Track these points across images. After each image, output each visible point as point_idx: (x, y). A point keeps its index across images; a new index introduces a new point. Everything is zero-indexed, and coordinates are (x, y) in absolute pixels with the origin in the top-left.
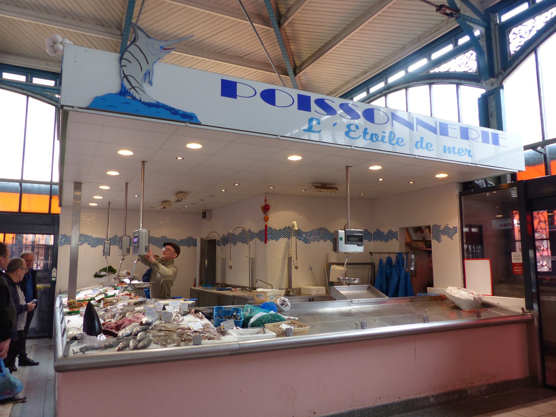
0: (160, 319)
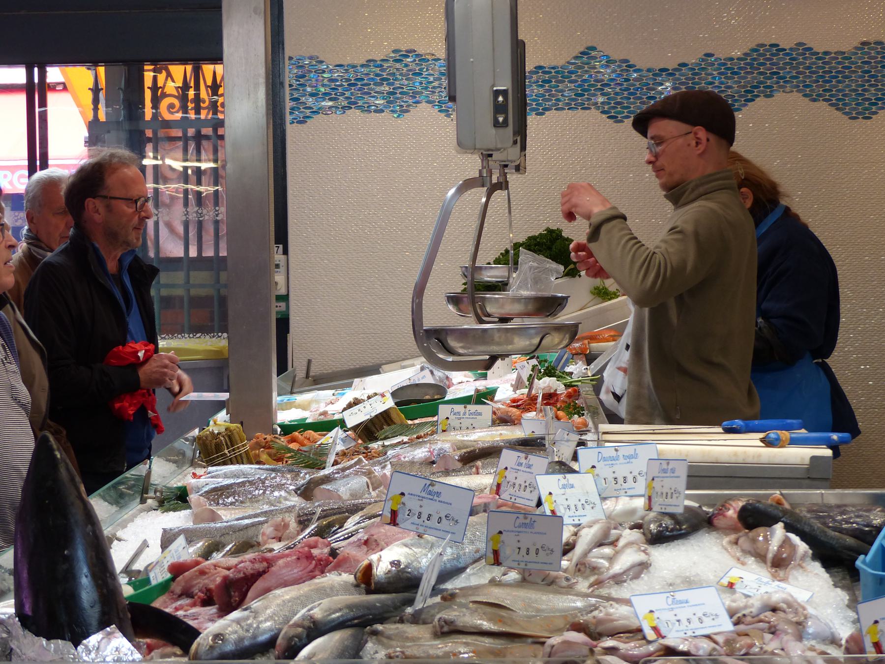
0: (496, 553)
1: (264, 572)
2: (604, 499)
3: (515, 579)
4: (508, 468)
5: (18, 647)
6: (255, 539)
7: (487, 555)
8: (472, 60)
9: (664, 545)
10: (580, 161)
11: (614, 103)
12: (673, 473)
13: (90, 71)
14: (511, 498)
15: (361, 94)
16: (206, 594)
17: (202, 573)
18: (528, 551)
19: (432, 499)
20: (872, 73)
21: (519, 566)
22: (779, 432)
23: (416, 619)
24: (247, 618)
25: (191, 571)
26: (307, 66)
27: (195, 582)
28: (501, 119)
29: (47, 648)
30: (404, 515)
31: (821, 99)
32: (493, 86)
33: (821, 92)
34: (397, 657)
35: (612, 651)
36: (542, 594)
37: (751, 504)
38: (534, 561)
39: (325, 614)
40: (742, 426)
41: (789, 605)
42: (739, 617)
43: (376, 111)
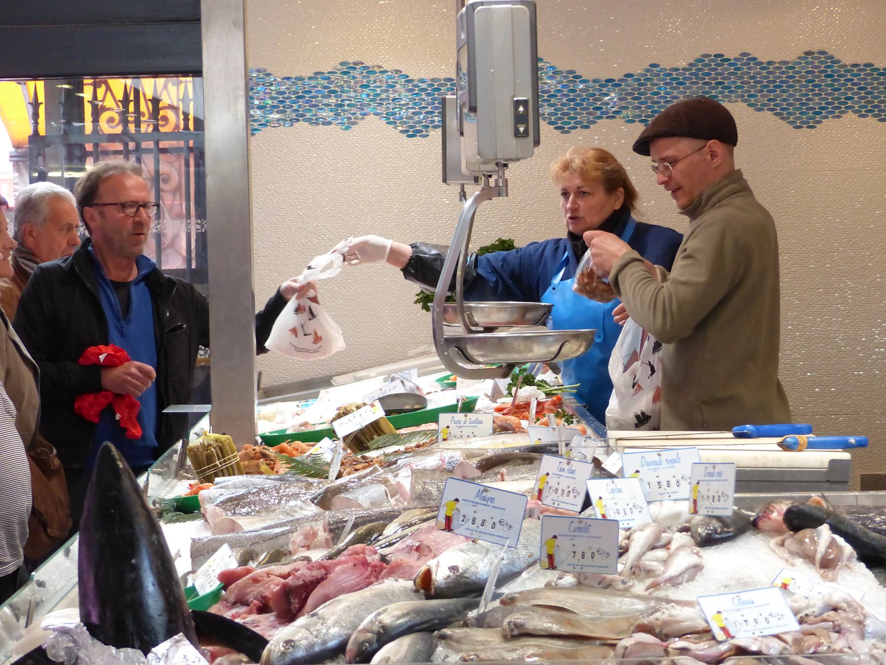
0: (551, 557)
1: (323, 579)
2: (649, 503)
3: (571, 583)
4: (550, 474)
5: (86, 656)
6: (285, 548)
7: (542, 559)
8: (492, 71)
9: (713, 547)
10: (528, 171)
11: (561, 114)
12: (720, 476)
13: (20, 85)
14: (554, 503)
15: (309, 106)
16: (261, 601)
17: (255, 581)
18: (583, 555)
19: (485, 505)
20: (816, 83)
21: (575, 570)
22: (797, 436)
23: (481, 622)
24: (316, 624)
25: (243, 578)
26: (254, 79)
27: (249, 590)
28: (522, 129)
29: (117, 656)
30: (458, 520)
31: (766, 108)
32: (514, 96)
33: (766, 102)
34: (472, 660)
35: (684, 651)
36: (603, 597)
37: (796, 507)
38: (590, 564)
39: (393, 619)
40: (752, 430)
41: (849, 605)
42: (801, 617)
43: (324, 124)
